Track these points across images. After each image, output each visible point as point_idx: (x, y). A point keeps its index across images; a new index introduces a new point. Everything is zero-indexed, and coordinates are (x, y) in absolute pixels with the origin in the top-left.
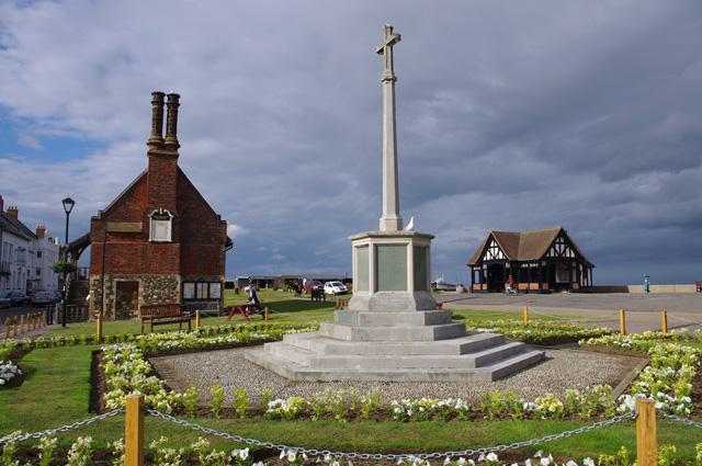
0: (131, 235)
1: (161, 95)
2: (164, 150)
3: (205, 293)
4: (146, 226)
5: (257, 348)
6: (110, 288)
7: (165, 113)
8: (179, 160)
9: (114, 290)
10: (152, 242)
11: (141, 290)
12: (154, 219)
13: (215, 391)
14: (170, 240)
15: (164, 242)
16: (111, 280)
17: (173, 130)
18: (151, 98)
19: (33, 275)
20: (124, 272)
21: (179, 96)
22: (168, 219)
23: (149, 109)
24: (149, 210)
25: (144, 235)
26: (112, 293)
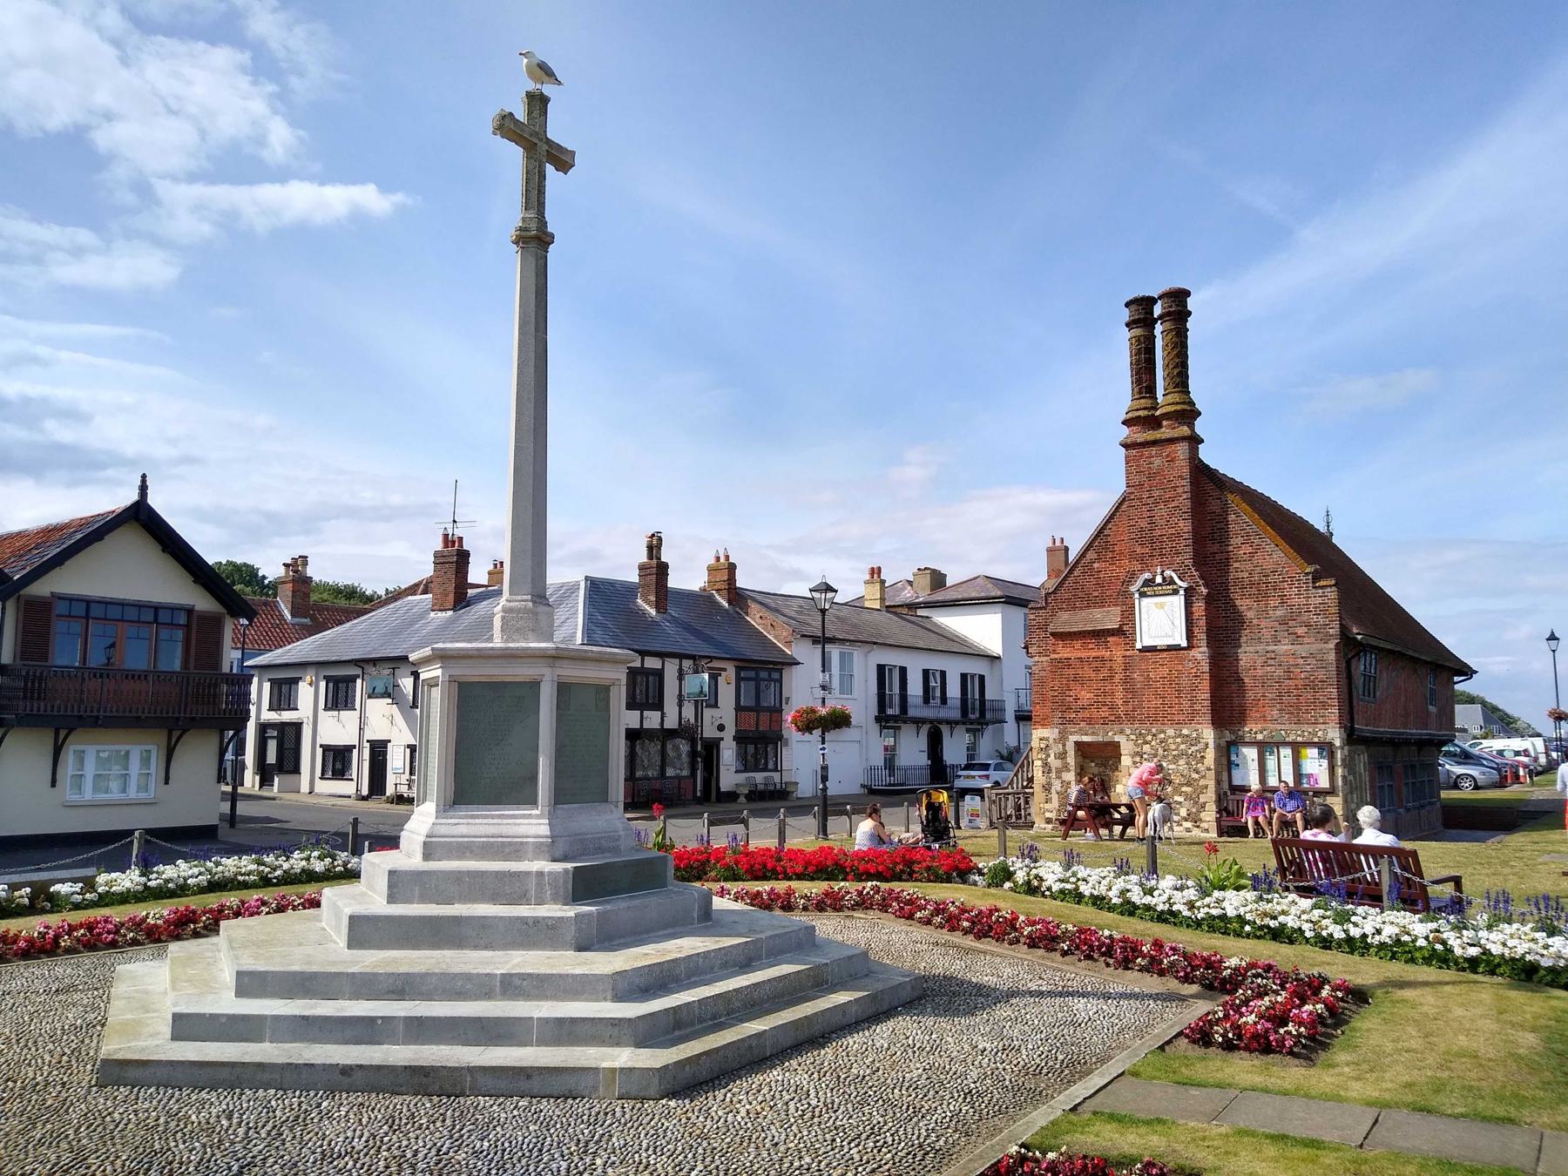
0: (1100, 635)
1: (1147, 302)
2: (1162, 414)
3: (1271, 762)
4: (1129, 614)
5: (267, 1061)
6: (1062, 756)
7: (1159, 343)
8: (1127, 319)
9: (1071, 760)
10: (1146, 649)
11: (1126, 761)
12: (1143, 595)
13: (1256, 1062)
14: (1184, 644)
15: (1170, 648)
16: (1062, 739)
17: (1180, 379)
18: (1126, 315)
19: (1256, 855)
20: (1090, 721)
21: (1187, 293)
22: (1175, 592)
23: (1121, 342)
24: (1132, 576)
25: (1124, 631)
26: (1066, 768)
